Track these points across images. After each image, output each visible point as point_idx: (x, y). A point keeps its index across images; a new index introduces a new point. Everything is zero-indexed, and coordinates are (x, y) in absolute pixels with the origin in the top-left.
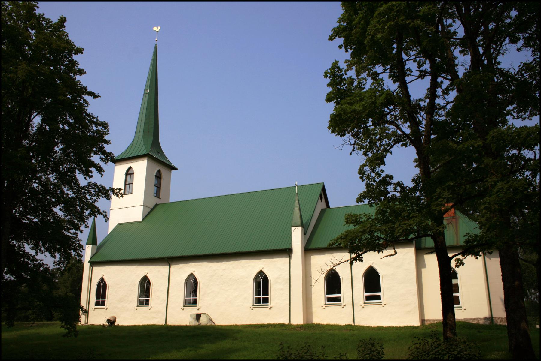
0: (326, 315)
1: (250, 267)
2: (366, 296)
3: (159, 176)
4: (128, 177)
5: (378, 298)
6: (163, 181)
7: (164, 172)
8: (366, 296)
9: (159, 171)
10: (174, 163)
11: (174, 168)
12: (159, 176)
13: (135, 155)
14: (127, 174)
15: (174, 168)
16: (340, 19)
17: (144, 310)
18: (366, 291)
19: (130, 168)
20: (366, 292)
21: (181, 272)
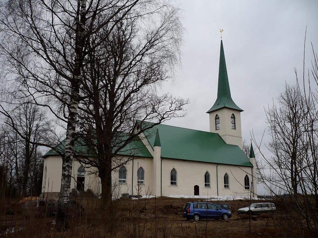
0: (204, 194)
1: (204, 169)
2: (119, 180)
3: (233, 117)
4: (217, 120)
5: (124, 181)
6: (236, 119)
7: (236, 114)
8: (119, 180)
9: (233, 114)
10: (240, 107)
11: (242, 111)
12: (233, 117)
13: (214, 110)
14: (216, 119)
15: (242, 111)
16: (178, 14)
17: (173, 188)
18: (84, 177)
19: (217, 115)
20: (84, 177)
21: (223, 171)
